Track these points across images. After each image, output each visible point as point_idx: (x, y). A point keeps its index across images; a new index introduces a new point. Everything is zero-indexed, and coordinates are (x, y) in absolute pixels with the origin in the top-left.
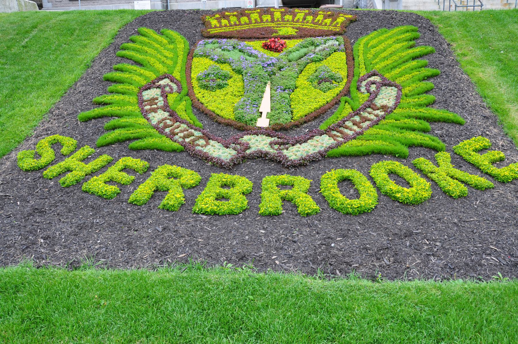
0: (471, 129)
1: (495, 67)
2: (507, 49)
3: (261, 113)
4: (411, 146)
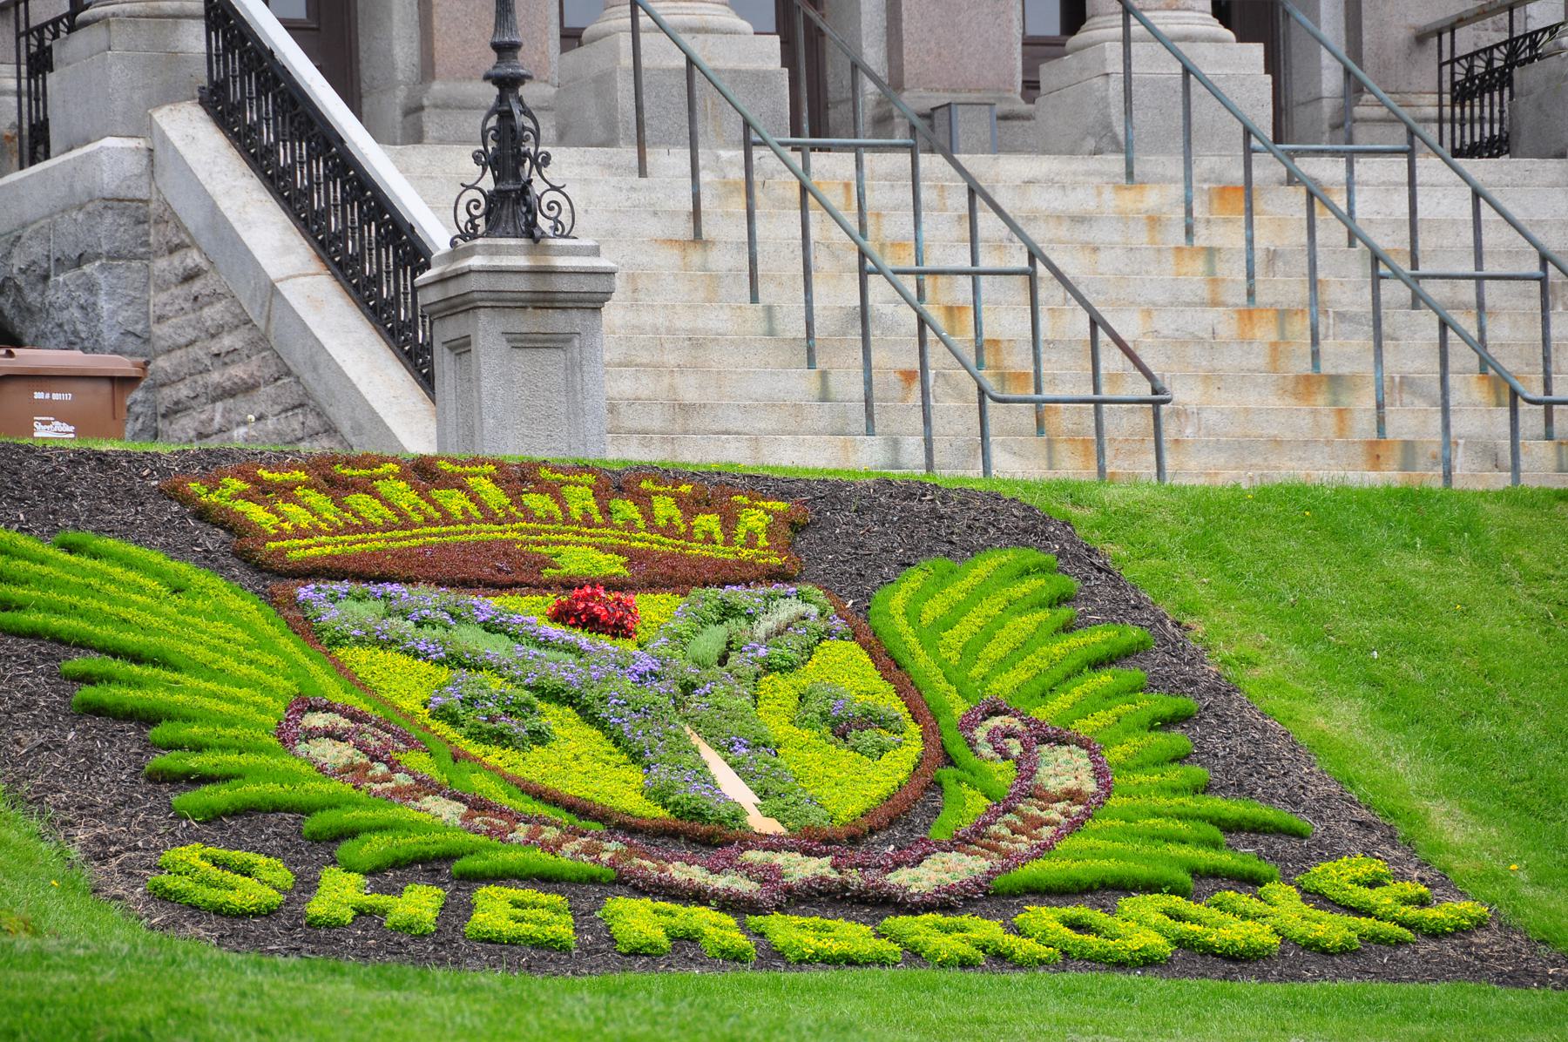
0: (1332, 845)
1: (1361, 702)
2: (1388, 642)
3: (360, 912)
4: (1196, 873)
